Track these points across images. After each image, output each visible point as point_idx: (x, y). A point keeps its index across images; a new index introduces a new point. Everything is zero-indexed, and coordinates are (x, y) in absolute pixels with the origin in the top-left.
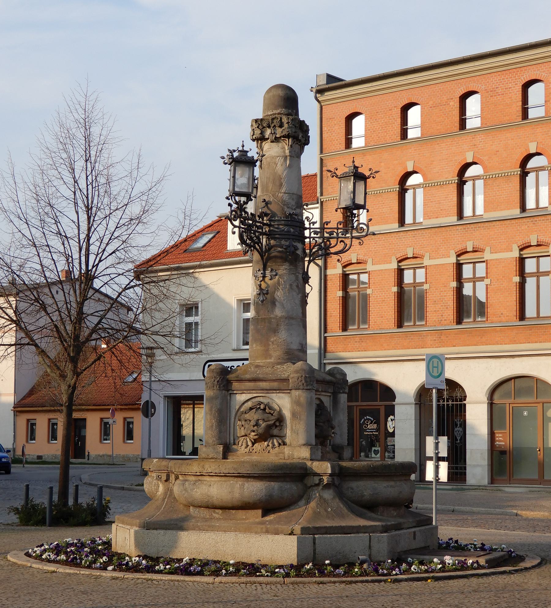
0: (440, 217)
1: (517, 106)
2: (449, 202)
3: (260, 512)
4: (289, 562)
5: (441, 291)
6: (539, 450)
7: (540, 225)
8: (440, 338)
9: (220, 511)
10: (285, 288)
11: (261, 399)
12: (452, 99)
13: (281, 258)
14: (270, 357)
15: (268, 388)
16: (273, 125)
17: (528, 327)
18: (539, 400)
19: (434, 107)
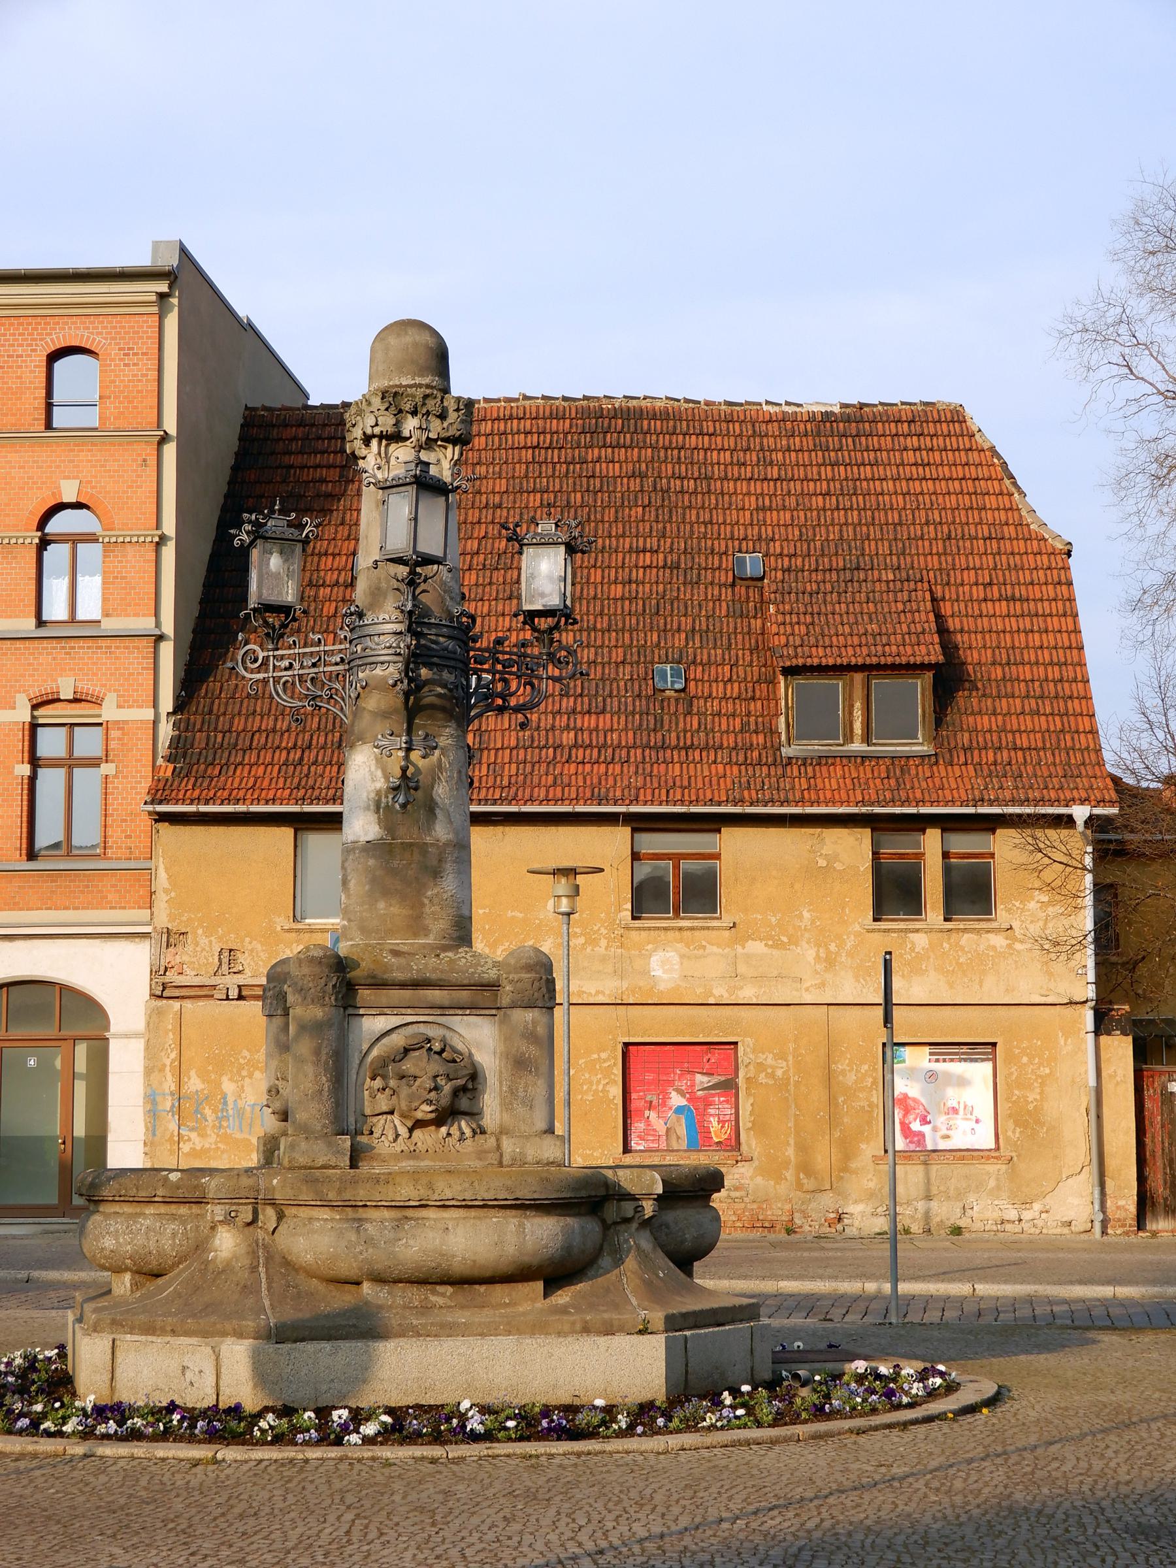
1: (35, 398)
3: (540, 1285)
4: (644, 1396)
6: (64, 1143)
7: (83, 658)
9: (449, 1290)
10: (451, 777)
13: (443, 709)
14: (426, 932)
15: (447, 1003)
16: (424, 411)
17: (48, 876)
18: (65, 1033)
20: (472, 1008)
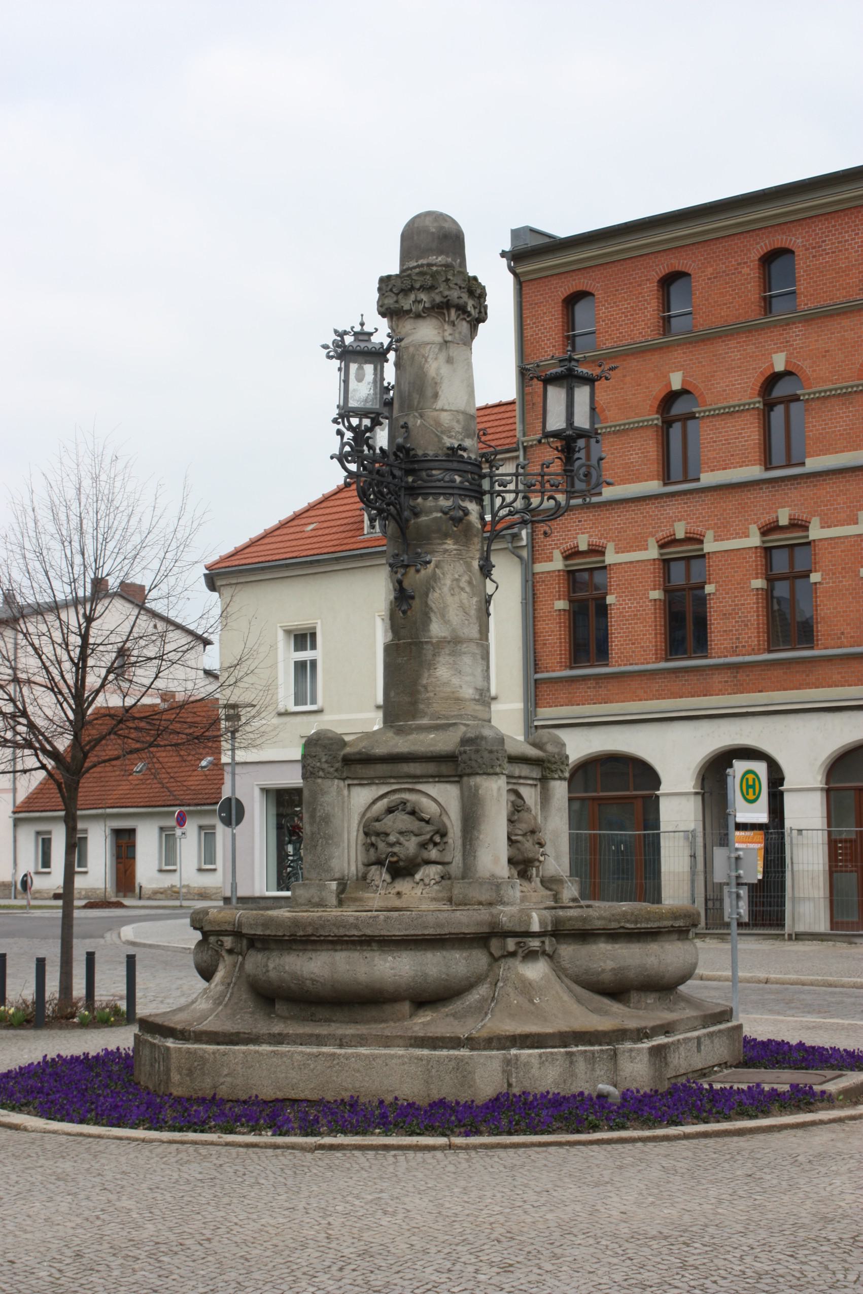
0: (730, 468)
2: (746, 441)
5: (736, 597)
8: (735, 677)
11: (406, 796)
12: (745, 263)
19: (715, 278)
20: (440, 778)
